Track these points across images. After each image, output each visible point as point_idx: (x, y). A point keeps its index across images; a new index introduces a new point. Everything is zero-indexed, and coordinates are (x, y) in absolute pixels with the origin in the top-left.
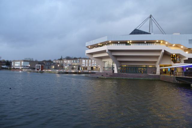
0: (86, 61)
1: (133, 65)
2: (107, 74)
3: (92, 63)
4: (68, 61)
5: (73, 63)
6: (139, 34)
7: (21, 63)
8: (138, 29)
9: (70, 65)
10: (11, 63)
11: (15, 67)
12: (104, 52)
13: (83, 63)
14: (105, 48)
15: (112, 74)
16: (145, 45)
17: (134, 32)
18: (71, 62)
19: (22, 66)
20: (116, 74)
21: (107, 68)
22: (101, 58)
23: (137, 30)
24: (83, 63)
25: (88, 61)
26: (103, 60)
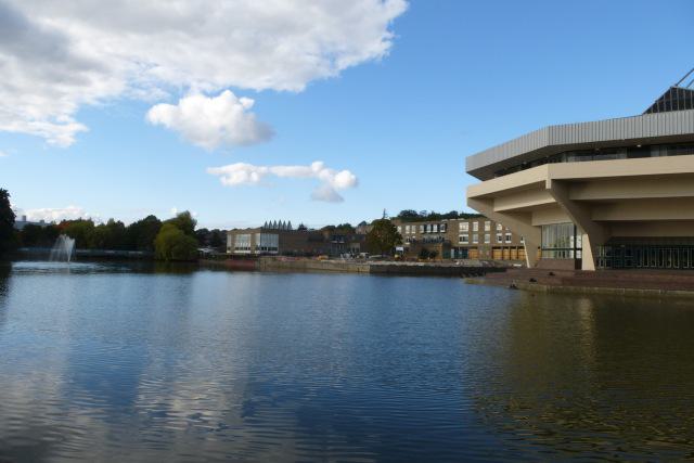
0: (471, 227)
1: (672, 239)
2: (551, 274)
3: (493, 230)
4: (408, 228)
5: (425, 232)
6: (682, 108)
7: (253, 240)
8: (683, 85)
9: (414, 242)
10: (226, 239)
11: (236, 252)
12: (537, 188)
13: (462, 233)
14: (542, 173)
15: (570, 275)
16: (660, 155)
17: (668, 103)
18: (418, 230)
19: (257, 249)
20: (588, 273)
21: (552, 252)
22: (525, 214)
23: (681, 90)
24: (462, 233)
25: (482, 227)
26: (536, 222)
